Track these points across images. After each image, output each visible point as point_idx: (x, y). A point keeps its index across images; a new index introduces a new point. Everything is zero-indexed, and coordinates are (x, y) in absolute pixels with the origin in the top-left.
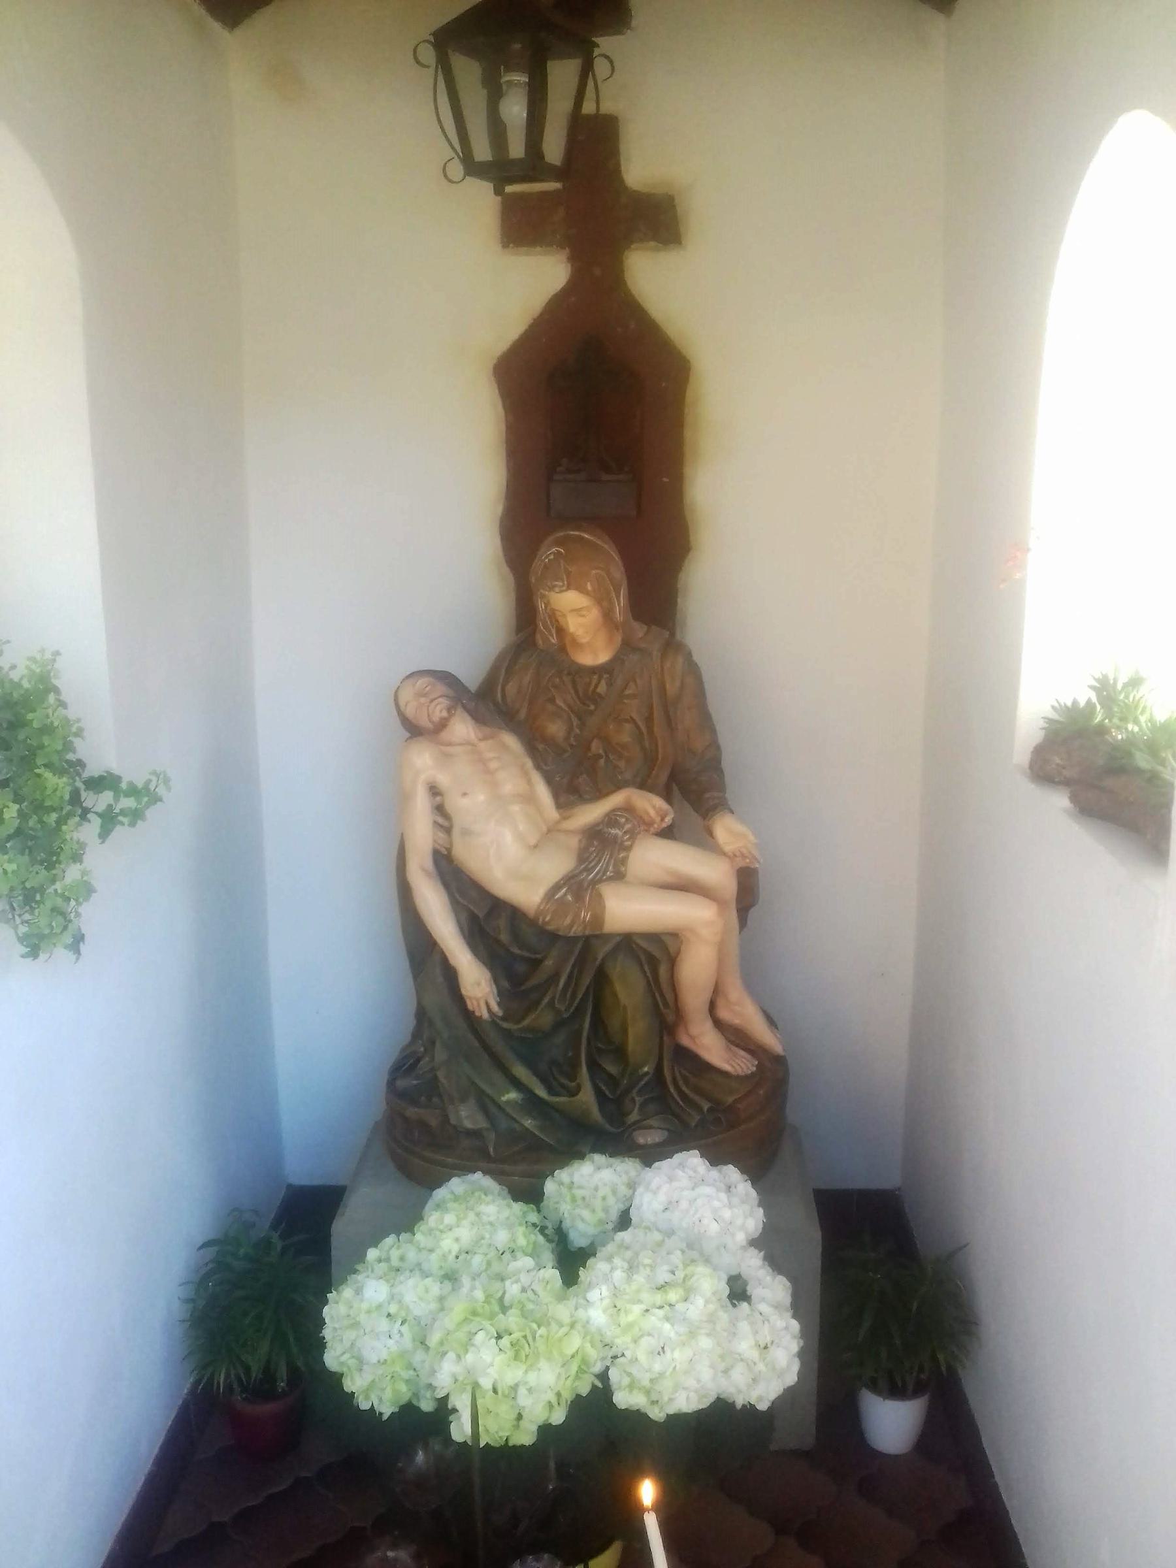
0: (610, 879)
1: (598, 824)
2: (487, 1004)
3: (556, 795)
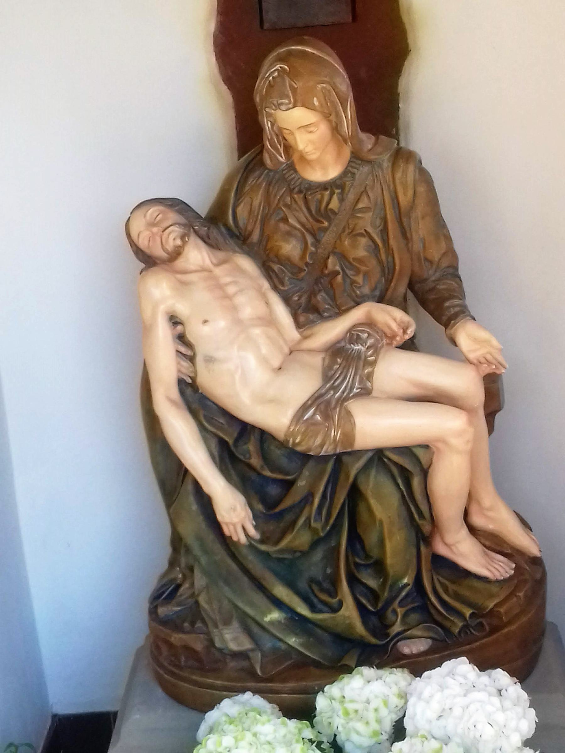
0: (357, 395)
1: (339, 342)
2: (244, 529)
3: (295, 317)
